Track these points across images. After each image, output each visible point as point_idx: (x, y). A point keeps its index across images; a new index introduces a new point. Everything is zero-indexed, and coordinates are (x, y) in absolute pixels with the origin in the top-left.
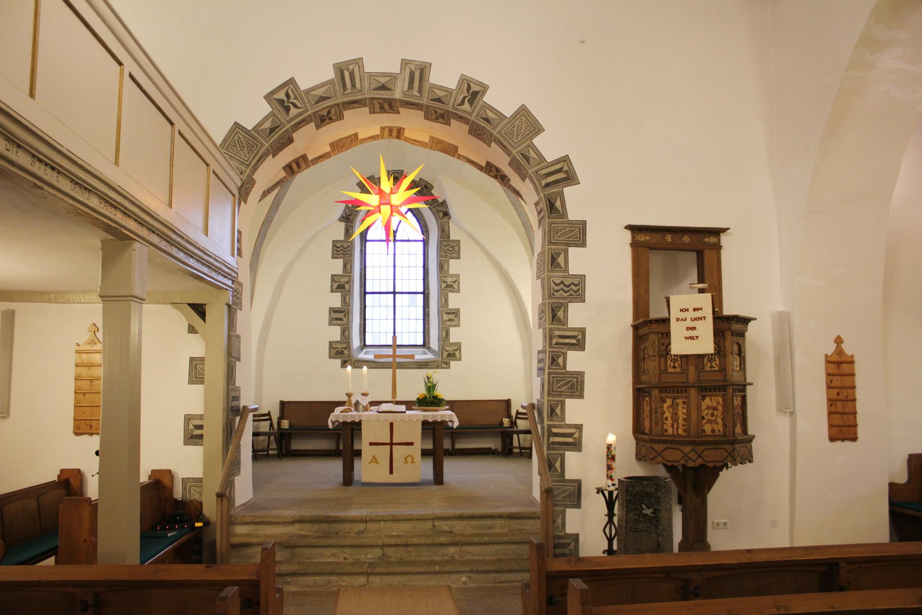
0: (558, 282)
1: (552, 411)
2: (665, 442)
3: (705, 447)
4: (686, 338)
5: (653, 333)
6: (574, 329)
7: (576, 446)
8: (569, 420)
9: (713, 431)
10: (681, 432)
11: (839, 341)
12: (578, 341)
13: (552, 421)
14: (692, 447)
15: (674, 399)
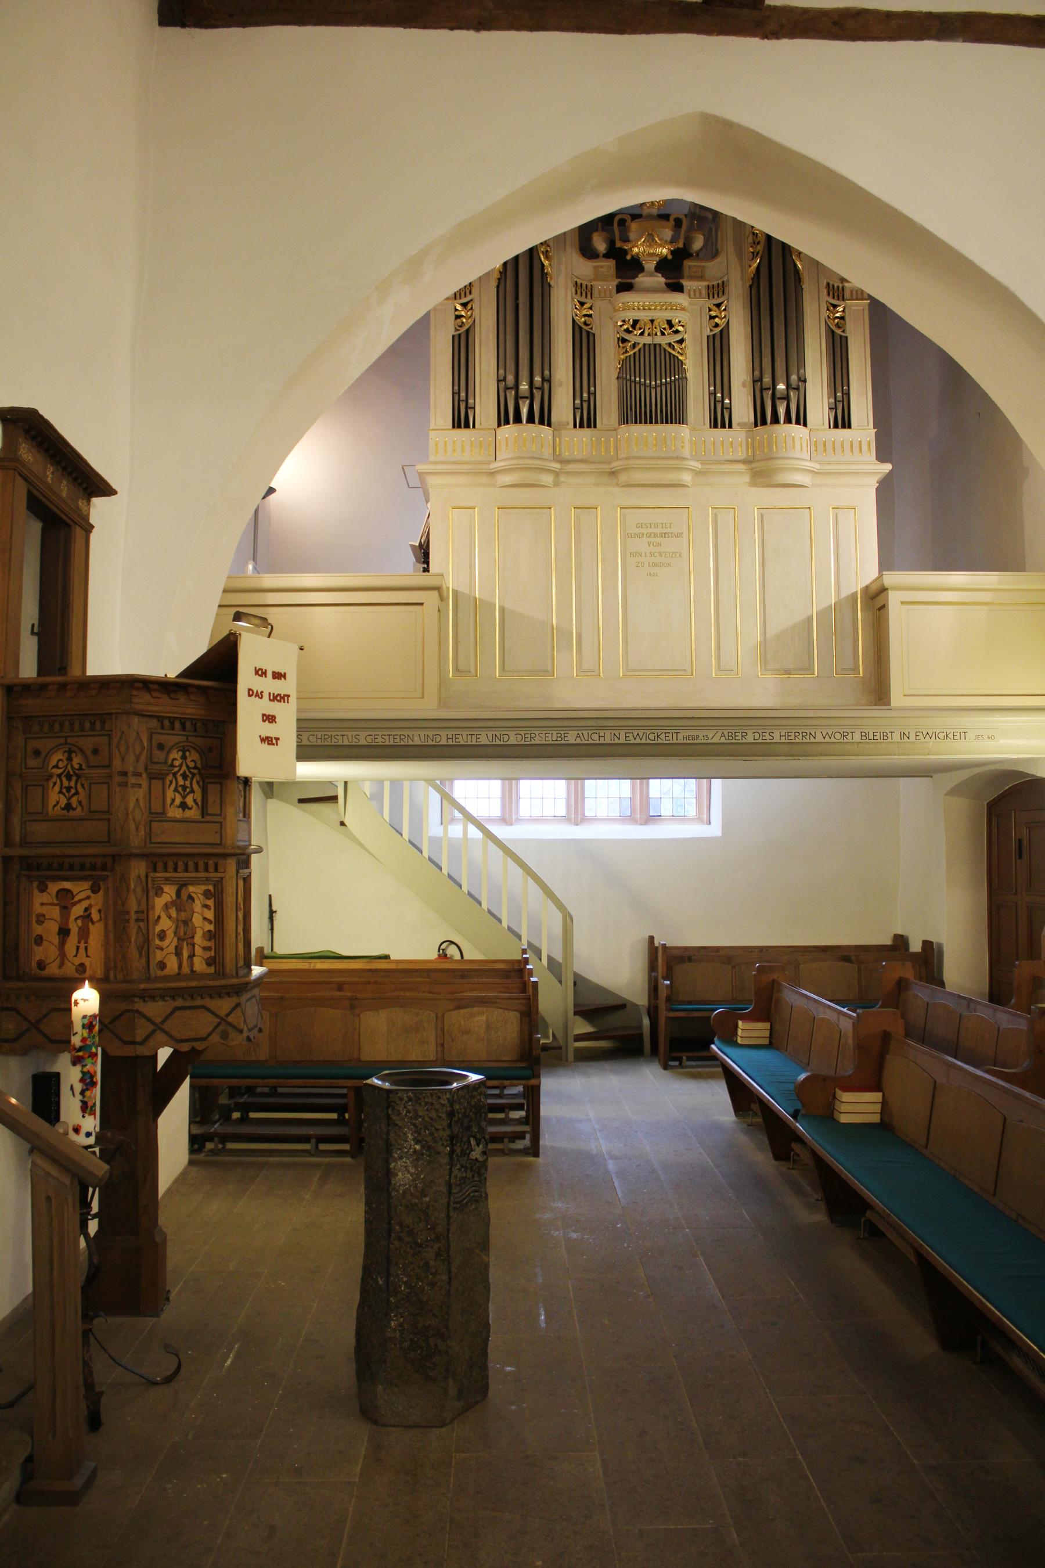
2: (173, 994)
5: (140, 714)
9: (39, 940)
10: (199, 965)
15: (182, 886)
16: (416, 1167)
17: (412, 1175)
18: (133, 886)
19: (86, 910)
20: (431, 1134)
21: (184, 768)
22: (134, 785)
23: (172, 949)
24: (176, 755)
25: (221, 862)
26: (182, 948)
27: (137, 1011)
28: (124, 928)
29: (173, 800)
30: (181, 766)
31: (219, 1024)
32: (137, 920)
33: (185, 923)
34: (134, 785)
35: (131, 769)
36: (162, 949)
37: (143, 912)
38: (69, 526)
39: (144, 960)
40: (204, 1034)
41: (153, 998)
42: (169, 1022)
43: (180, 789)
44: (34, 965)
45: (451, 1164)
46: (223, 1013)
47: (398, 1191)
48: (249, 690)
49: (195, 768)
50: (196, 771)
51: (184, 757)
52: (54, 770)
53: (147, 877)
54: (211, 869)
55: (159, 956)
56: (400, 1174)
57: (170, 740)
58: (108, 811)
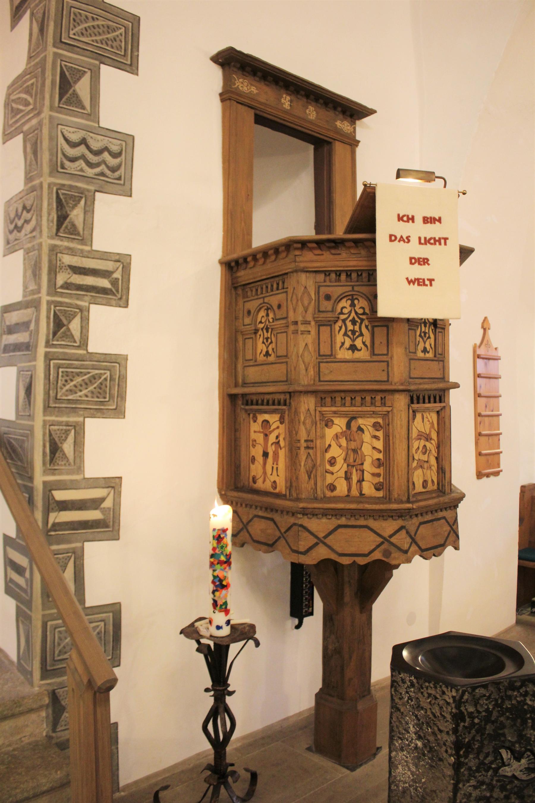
0: (75, 137)
1: (54, 449)
2: (337, 513)
3: (421, 519)
4: (410, 282)
5: (304, 271)
6: (104, 256)
7: (107, 527)
8: (94, 468)
10: (368, 489)
12: (114, 288)
13: (53, 472)
14: (400, 523)
16: (416, 766)
17: (413, 773)
18: (302, 419)
19: (277, 437)
20: (434, 733)
21: (353, 314)
22: (303, 333)
23: (342, 474)
24: (345, 303)
25: (389, 397)
26: (351, 474)
27: (301, 526)
29: (343, 344)
30: (350, 312)
31: (382, 543)
32: (307, 448)
33: (355, 451)
34: (303, 333)
35: (300, 319)
36: (332, 474)
37: (312, 441)
38: (329, 143)
39: (312, 482)
40: (366, 550)
41: (314, 515)
43: (349, 333)
45: (458, 779)
46: (386, 534)
47: (398, 786)
48: (391, 236)
49: (364, 314)
50: (364, 317)
51: (353, 305)
53: (316, 410)
54: (378, 403)
55: (329, 479)
56: (400, 767)
57: (337, 291)
58: (286, 356)
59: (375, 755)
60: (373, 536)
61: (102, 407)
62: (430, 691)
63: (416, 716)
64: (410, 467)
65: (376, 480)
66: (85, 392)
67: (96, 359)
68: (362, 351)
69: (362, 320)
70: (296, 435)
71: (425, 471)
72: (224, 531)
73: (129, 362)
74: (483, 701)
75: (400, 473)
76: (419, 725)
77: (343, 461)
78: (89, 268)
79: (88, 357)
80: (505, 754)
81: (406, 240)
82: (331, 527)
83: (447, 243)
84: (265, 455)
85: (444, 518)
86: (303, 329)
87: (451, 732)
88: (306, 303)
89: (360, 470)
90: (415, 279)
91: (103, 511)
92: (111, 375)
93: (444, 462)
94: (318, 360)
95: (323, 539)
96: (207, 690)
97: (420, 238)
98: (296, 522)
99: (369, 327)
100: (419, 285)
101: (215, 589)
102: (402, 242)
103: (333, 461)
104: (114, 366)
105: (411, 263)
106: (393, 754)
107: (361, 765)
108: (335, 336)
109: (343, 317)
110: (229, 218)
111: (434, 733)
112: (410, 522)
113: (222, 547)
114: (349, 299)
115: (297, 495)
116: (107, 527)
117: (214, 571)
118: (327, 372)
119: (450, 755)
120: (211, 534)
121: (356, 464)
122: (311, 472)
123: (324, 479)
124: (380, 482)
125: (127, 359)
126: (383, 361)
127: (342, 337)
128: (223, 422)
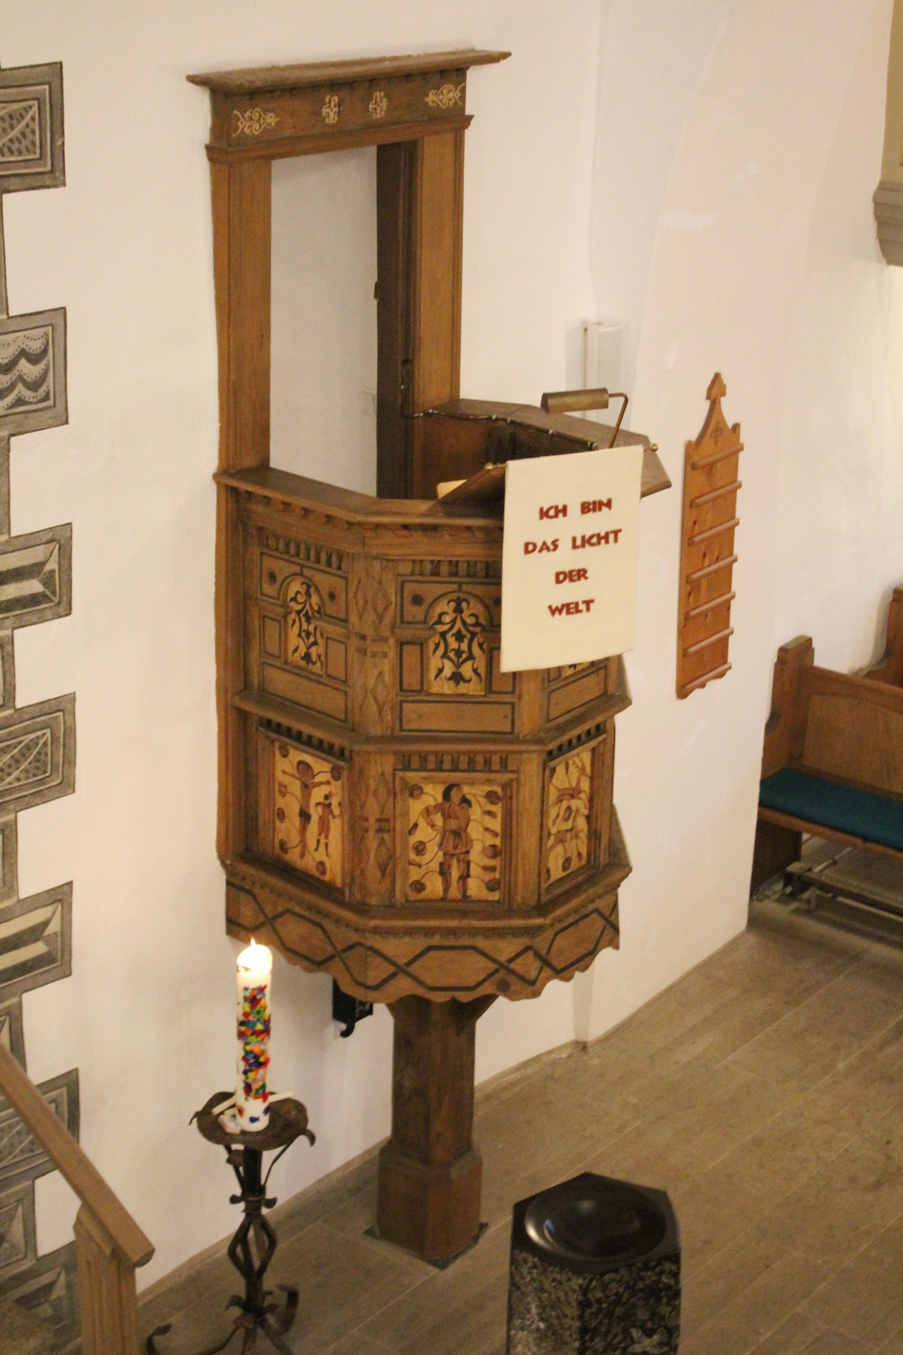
4: (553, 611)
11: (716, 390)
16: (538, 1346)
18: (372, 787)
19: (327, 797)
20: (558, 1317)
21: (458, 625)
23: (435, 866)
26: (450, 867)
28: (363, 838)
29: (441, 670)
30: (453, 622)
35: (370, 632)
36: (420, 866)
37: (388, 821)
39: (388, 881)
40: (472, 982)
42: (416, 964)
43: (452, 655)
44: (277, 845)
48: (527, 545)
51: (458, 610)
52: (292, 604)
53: (394, 776)
55: (414, 874)
57: (430, 591)
58: (345, 681)
59: (477, 1238)
60: (483, 962)
61: (42, 788)
62: (554, 1275)
63: (539, 1298)
64: (544, 847)
65: (488, 876)
66: (16, 774)
67: (28, 716)
68: (471, 683)
69: (473, 635)
70: (362, 809)
71: (567, 844)
72: (262, 990)
73: (77, 703)
74: (613, 1285)
75: (527, 867)
76: (542, 1307)
77: (436, 848)
78: (8, 570)
79: (16, 717)
80: (635, 1333)
81: (552, 547)
82: (418, 950)
83: (619, 539)
84: (305, 816)
85: (596, 910)
86: (374, 649)
87: (576, 1318)
88: (381, 607)
89: (464, 861)
90: (563, 606)
91: (48, 941)
92: (52, 733)
93: (599, 822)
94: (399, 698)
95: (405, 967)
96: (234, 1200)
97: (574, 539)
98: (362, 941)
99: (485, 646)
100: (568, 613)
101: (247, 1068)
102: (545, 552)
103: (421, 848)
104: (56, 718)
105: (558, 581)
106: (512, 1332)
107: (456, 1258)
108: (428, 659)
109: (441, 628)
110: (232, 398)
111: (558, 1317)
112: (541, 938)
113: (259, 1012)
114: (452, 600)
115: (364, 897)
116: (53, 961)
117: (247, 1044)
118: (414, 716)
119: (576, 1340)
120: (241, 995)
121: (457, 851)
122: (386, 867)
123: (406, 874)
124: (494, 879)
125: (75, 700)
126: (506, 703)
127: (440, 661)
128: (227, 751)
